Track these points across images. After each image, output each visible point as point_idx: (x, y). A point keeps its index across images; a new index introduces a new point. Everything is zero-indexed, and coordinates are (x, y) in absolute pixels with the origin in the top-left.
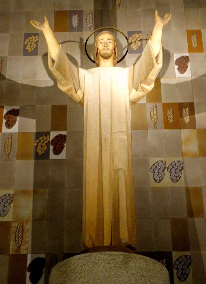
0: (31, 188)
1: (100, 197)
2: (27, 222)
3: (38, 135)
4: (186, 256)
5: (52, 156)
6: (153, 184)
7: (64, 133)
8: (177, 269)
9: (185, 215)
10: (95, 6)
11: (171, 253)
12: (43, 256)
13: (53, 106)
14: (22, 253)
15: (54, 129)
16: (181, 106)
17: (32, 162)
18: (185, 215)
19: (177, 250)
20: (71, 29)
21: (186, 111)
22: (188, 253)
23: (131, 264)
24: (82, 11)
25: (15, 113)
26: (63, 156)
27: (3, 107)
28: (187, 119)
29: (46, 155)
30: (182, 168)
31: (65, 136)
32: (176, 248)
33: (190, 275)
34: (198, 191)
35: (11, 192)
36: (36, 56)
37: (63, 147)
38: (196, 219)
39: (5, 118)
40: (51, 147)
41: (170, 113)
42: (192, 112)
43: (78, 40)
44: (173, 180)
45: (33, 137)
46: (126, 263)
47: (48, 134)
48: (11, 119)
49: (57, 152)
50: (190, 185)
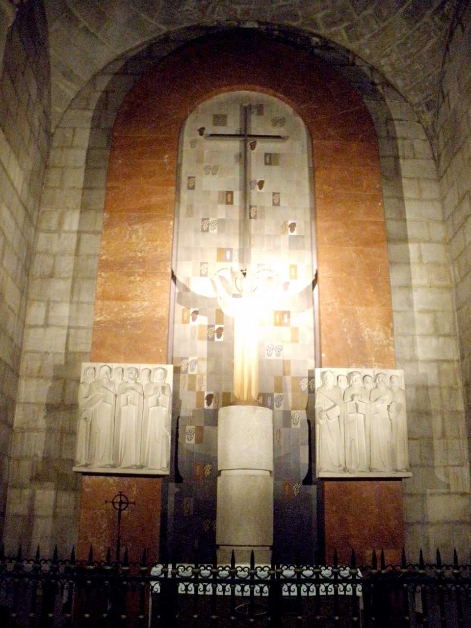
0: (205, 356)
1: (243, 377)
2: (204, 375)
3: (209, 326)
4: (280, 396)
5: (216, 339)
6: (267, 357)
7: (222, 326)
8: (276, 402)
9: (281, 374)
10: (240, 246)
11: (273, 394)
12: (212, 393)
13: (217, 310)
14: (202, 391)
15: (217, 323)
16: (284, 313)
17: (206, 342)
18: (281, 374)
19: (278, 392)
20: (225, 260)
21: (286, 316)
22: (281, 394)
23: (257, 411)
24: (232, 249)
25: (196, 313)
26: (221, 339)
27: (190, 309)
28: (286, 320)
29: (212, 339)
30: (282, 349)
31: (223, 328)
32: (276, 391)
33: (282, 405)
34: (288, 362)
35: (196, 358)
36: (225, 391)
37: (221, 335)
38: (286, 377)
39: (191, 315)
40: (216, 334)
41: (278, 316)
42: (289, 317)
43: (230, 268)
44: (277, 355)
45: (206, 328)
46: (254, 410)
47: (213, 326)
48: (195, 317)
49: (219, 336)
50: (285, 359)
